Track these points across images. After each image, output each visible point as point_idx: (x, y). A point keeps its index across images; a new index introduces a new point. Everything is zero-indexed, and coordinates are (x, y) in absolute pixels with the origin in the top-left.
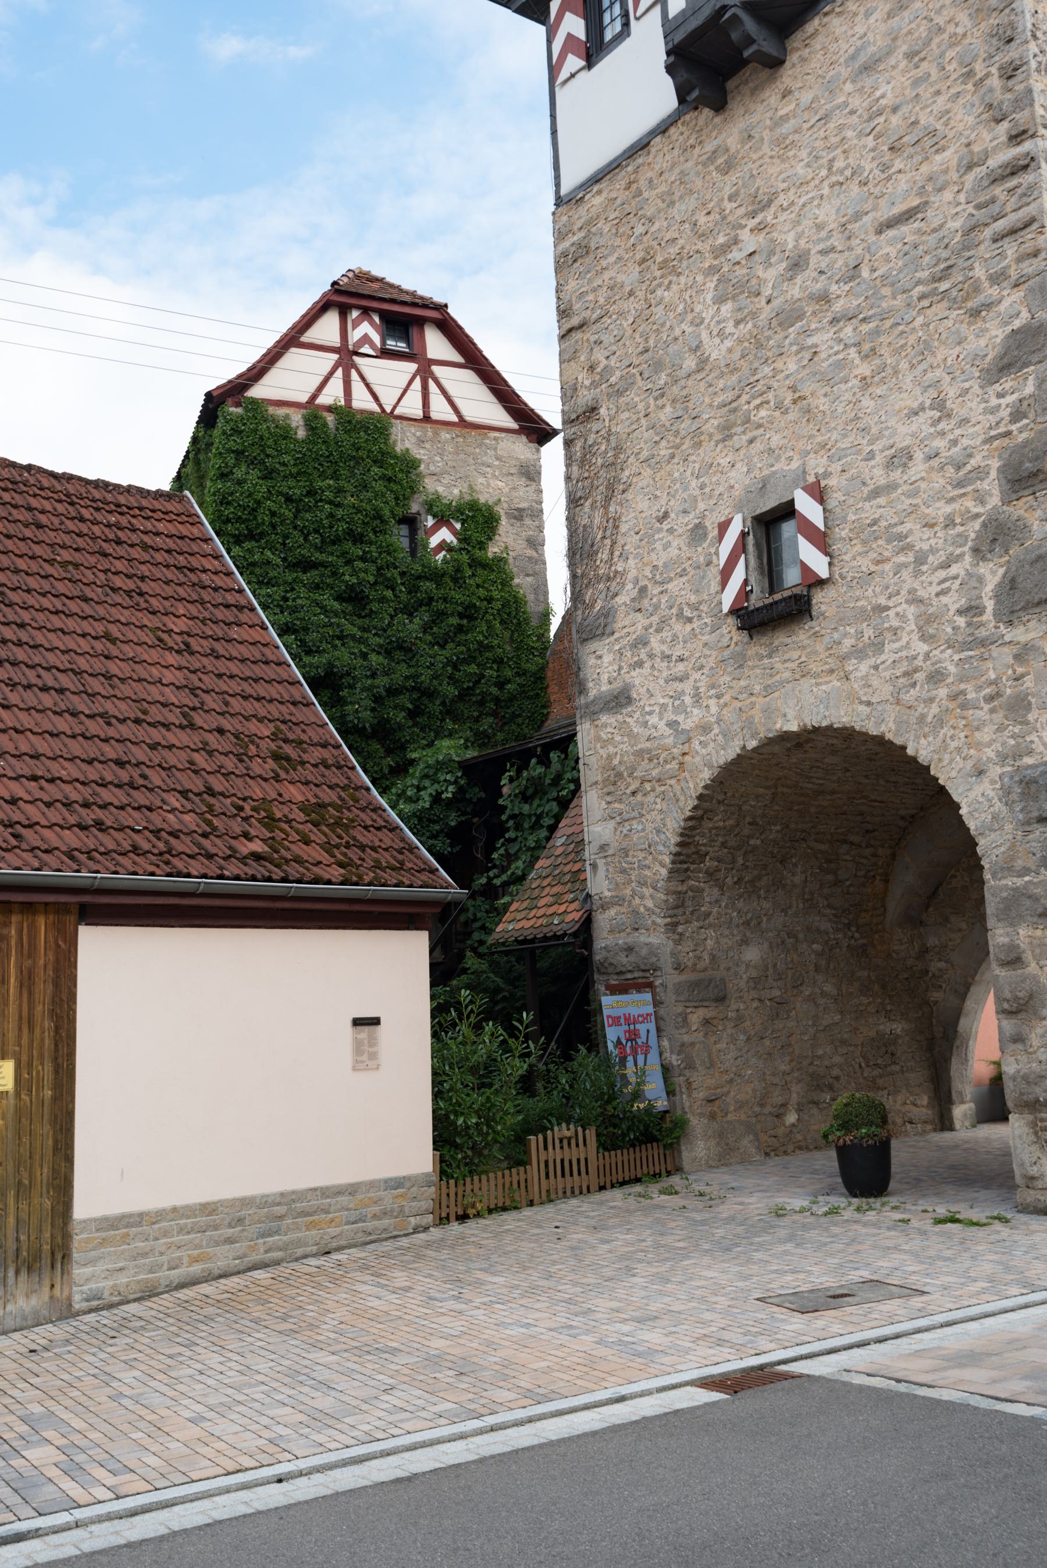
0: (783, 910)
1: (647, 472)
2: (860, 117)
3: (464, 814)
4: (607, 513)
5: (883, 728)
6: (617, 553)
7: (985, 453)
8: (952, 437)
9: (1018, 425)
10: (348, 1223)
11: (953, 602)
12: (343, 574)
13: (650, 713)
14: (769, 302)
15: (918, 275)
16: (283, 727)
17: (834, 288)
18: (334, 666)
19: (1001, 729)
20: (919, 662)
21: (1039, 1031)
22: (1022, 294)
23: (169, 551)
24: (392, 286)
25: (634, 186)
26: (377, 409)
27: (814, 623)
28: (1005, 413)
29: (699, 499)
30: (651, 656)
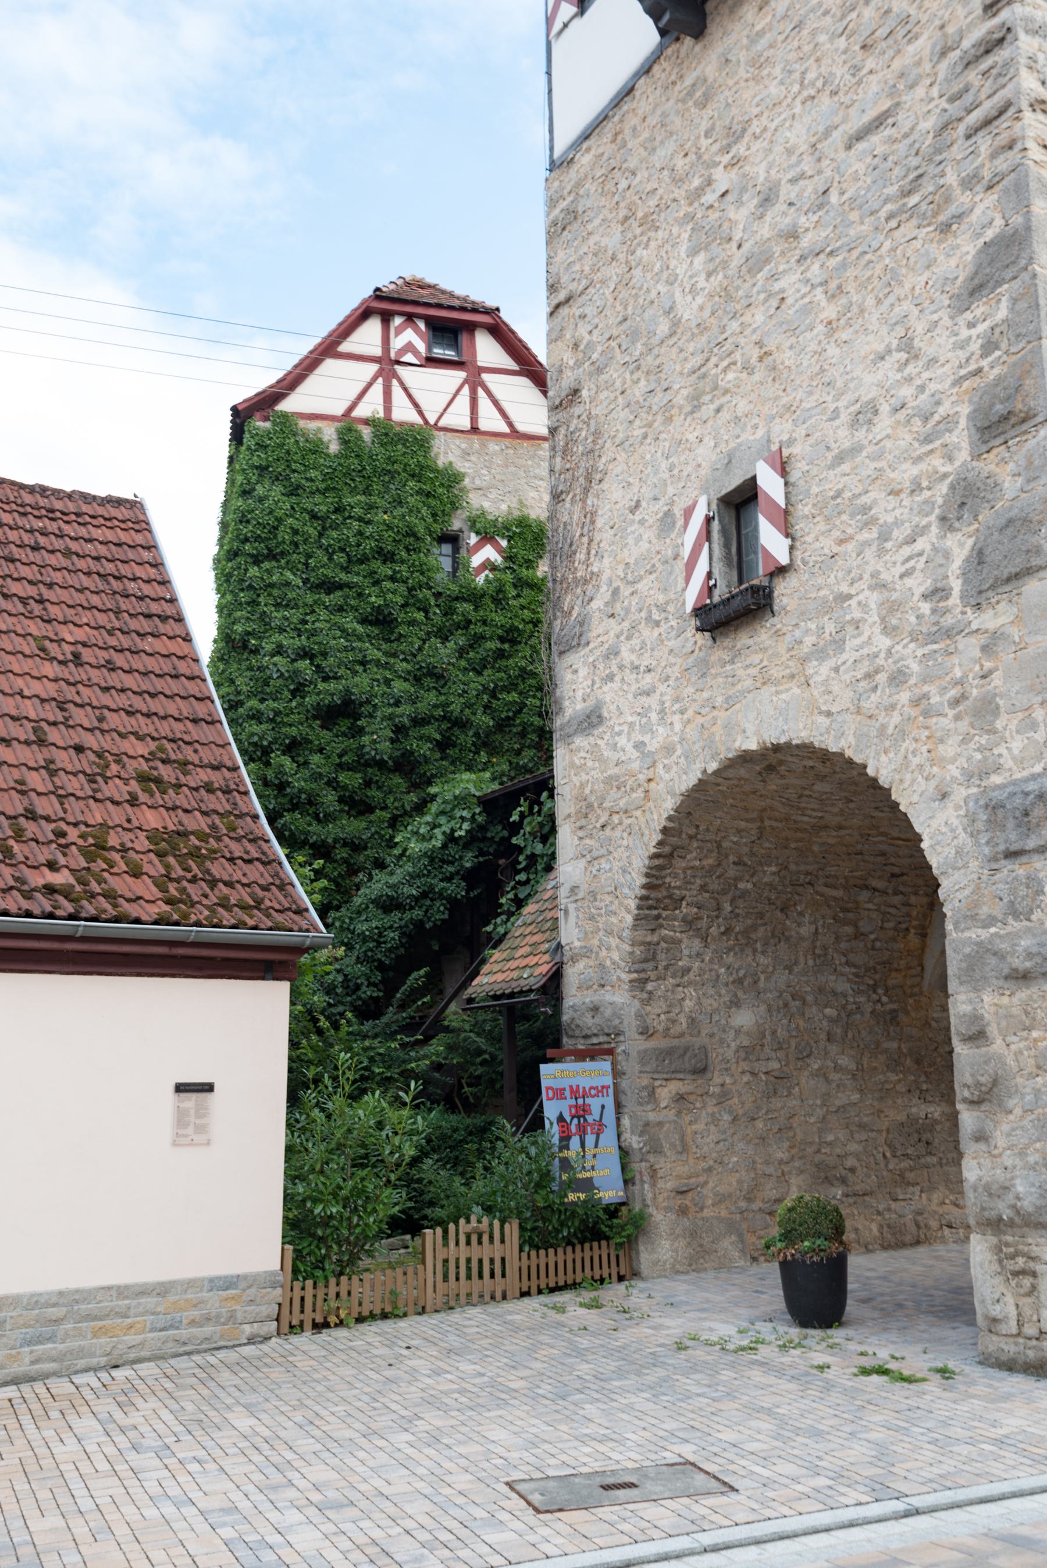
0: (786, 967)
1: (622, 457)
2: (833, 16)
3: (482, 853)
4: (584, 508)
5: (843, 743)
6: (593, 552)
7: (954, 398)
8: (919, 382)
9: (990, 359)
10: (153, 1330)
11: (918, 584)
12: (370, 595)
13: (619, 734)
14: (739, 246)
15: (886, 191)
16: (168, 746)
17: (803, 219)
18: (352, 694)
19: (966, 740)
20: (880, 661)
21: (1005, 1127)
22: (996, 197)
23: (97, 559)
24: (443, 292)
25: (620, 137)
26: (420, 421)
27: (775, 620)
28: (975, 346)
29: (669, 482)
30: (621, 667)
